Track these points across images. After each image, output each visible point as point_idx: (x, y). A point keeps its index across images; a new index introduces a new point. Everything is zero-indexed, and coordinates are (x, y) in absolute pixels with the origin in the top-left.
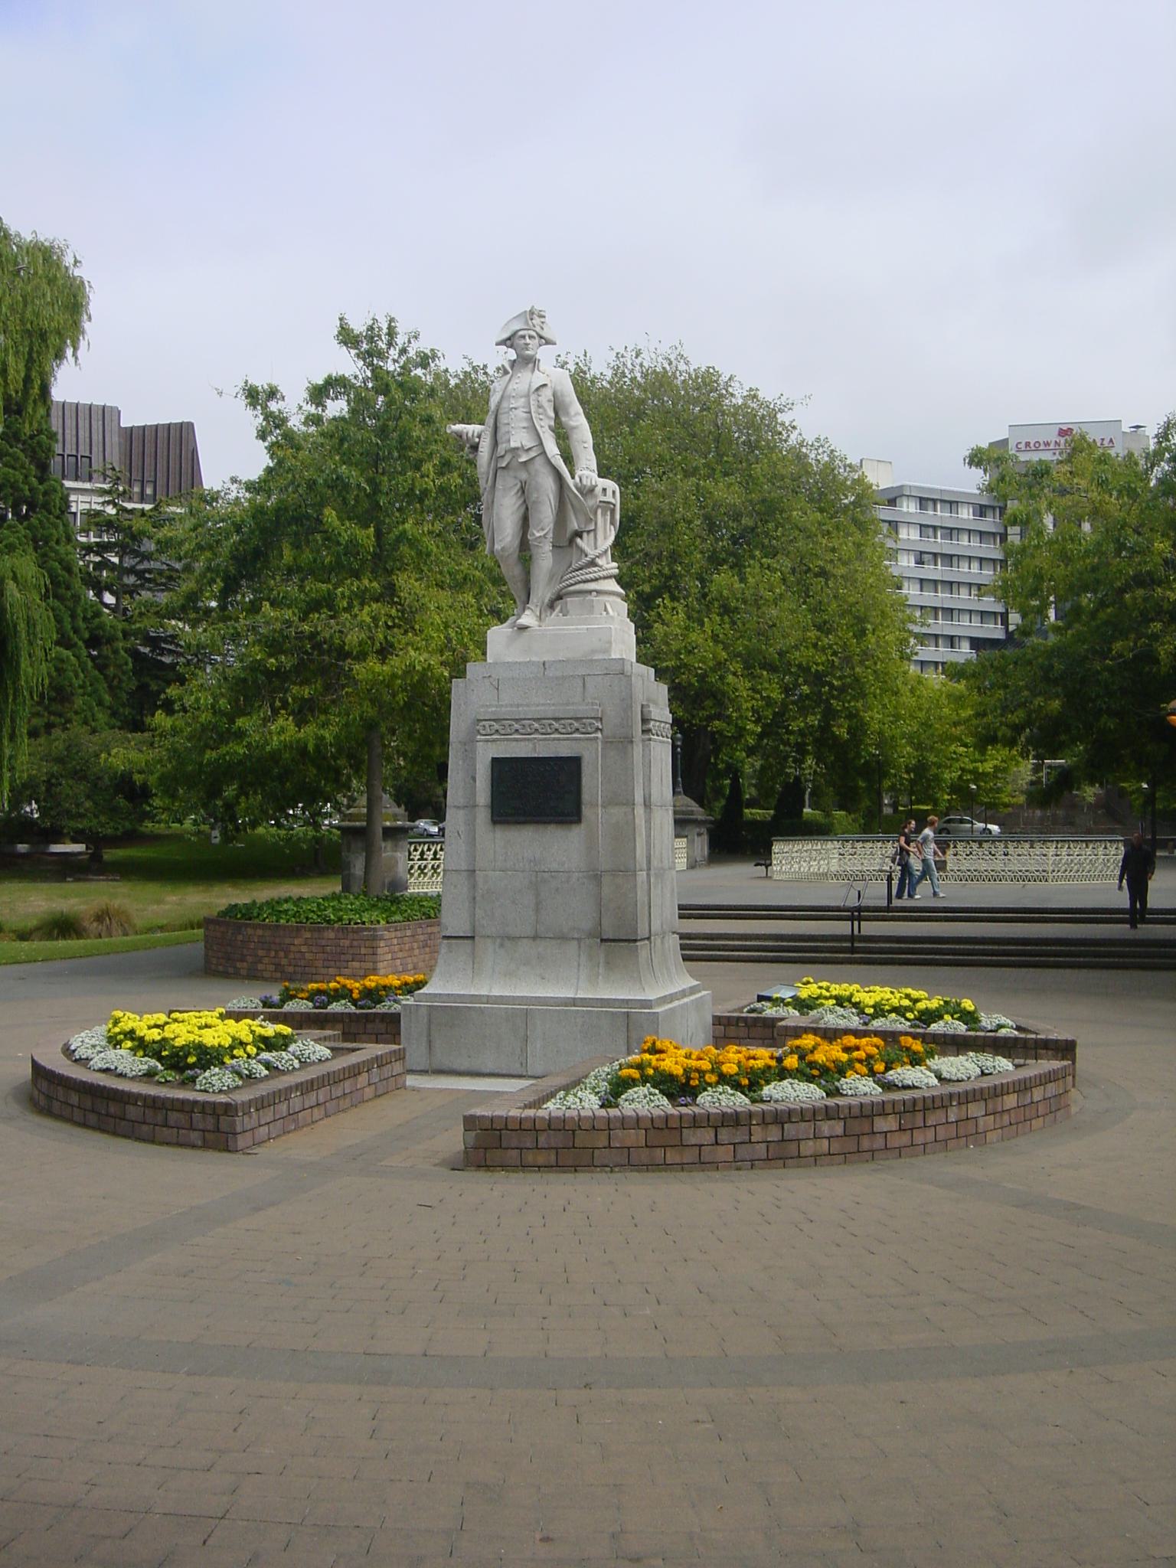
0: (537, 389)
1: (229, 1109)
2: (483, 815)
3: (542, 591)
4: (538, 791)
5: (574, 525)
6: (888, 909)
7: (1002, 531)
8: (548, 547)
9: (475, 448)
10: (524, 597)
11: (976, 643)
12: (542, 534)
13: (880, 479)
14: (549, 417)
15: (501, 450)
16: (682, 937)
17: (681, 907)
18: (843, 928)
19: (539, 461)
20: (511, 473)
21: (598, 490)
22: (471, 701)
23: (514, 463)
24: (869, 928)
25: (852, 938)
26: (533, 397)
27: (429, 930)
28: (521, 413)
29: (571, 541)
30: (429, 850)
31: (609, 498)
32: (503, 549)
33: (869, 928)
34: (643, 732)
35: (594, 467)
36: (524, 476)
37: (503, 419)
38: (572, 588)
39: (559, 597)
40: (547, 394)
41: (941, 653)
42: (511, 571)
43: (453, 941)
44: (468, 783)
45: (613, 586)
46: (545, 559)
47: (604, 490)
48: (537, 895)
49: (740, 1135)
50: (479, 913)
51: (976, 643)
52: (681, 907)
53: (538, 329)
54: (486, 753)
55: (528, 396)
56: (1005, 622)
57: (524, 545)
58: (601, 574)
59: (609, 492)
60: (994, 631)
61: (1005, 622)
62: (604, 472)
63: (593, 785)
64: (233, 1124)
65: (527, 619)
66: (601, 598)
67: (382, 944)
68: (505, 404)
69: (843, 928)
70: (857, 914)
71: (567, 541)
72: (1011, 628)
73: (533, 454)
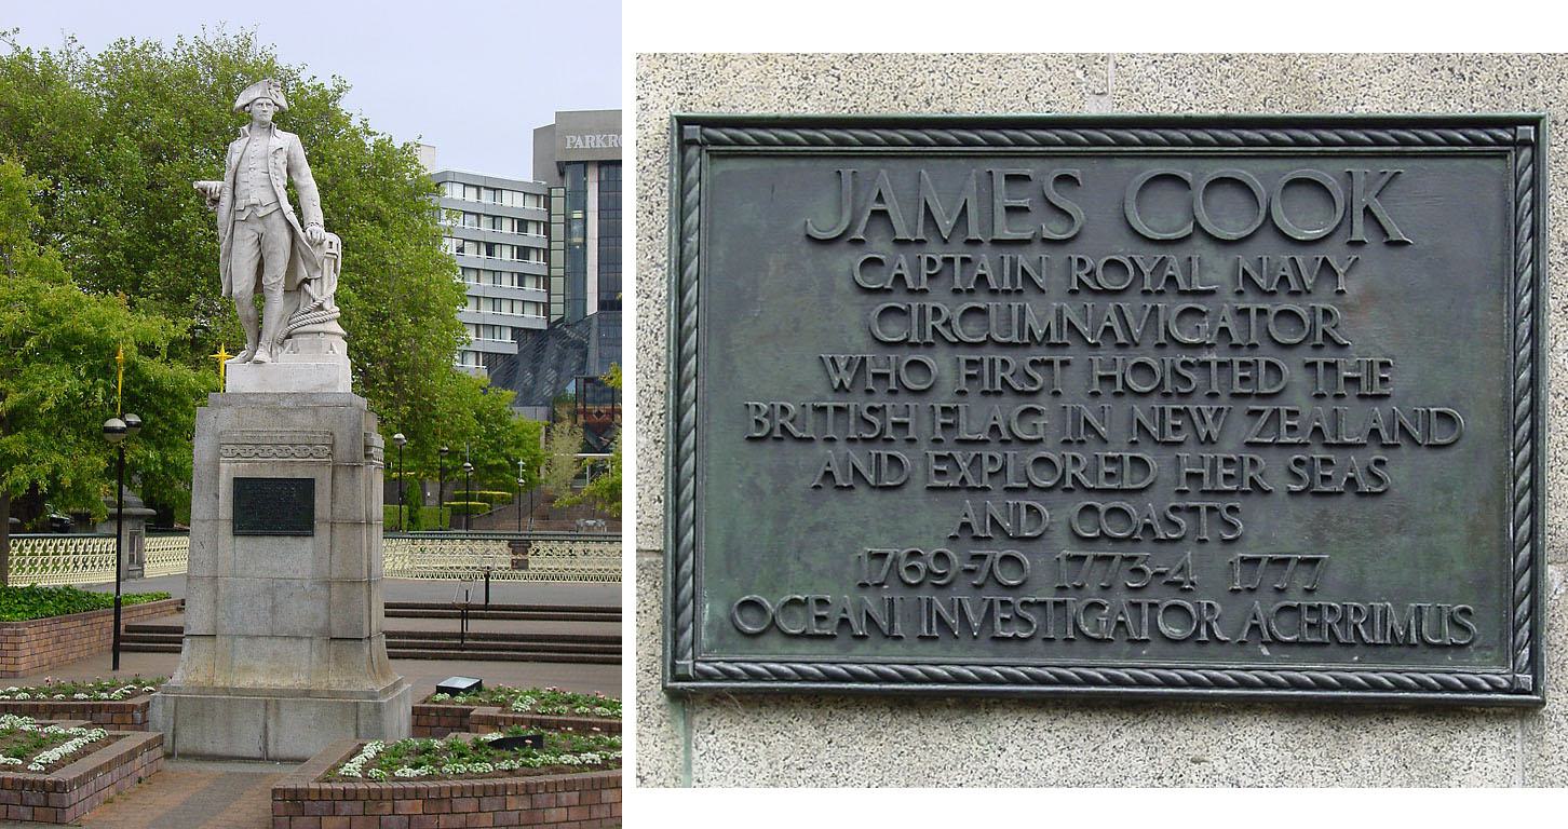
0: (275, 153)
1: (57, 786)
2: (226, 528)
3: (273, 325)
4: (275, 508)
5: (303, 273)
6: (486, 607)
7: (546, 220)
8: (280, 291)
9: (216, 201)
10: (255, 336)
11: (517, 333)
12: (275, 280)
13: (432, 163)
14: (283, 178)
15: (240, 204)
16: (389, 635)
17: (387, 606)
18: (453, 626)
19: (276, 216)
20: (250, 226)
21: (326, 243)
22: (210, 429)
23: (252, 218)
24: (475, 626)
25: (462, 636)
26: (271, 159)
27: (63, 625)
28: (259, 174)
29: (300, 286)
30: (27, 545)
31: (334, 251)
32: (241, 293)
33: (475, 626)
34: (366, 456)
35: (322, 223)
36: (259, 228)
37: (242, 177)
38: (302, 329)
39: (289, 336)
40: (282, 157)
41: (487, 343)
42: (244, 310)
43: (196, 639)
44: (211, 504)
45: (336, 327)
46: (277, 303)
47: (331, 243)
48: (274, 599)
49: (496, 803)
50: (221, 615)
51: (517, 333)
52: (387, 606)
53: (274, 97)
54: (228, 471)
55: (266, 157)
56: (547, 313)
57: (258, 286)
58: (327, 317)
59: (334, 245)
60: (534, 320)
61: (547, 313)
62: (329, 227)
63: (322, 505)
64: (62, 800)
65: (261, 355)
66: (329, 337)
67: (24, 639)
68: (244, 165)
69: (453, 626)
70: (465, 612)
71: (296, 288)
72: (553, 319)
73: (269, 210)
